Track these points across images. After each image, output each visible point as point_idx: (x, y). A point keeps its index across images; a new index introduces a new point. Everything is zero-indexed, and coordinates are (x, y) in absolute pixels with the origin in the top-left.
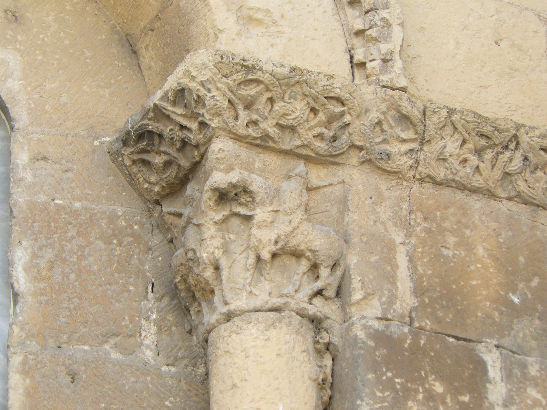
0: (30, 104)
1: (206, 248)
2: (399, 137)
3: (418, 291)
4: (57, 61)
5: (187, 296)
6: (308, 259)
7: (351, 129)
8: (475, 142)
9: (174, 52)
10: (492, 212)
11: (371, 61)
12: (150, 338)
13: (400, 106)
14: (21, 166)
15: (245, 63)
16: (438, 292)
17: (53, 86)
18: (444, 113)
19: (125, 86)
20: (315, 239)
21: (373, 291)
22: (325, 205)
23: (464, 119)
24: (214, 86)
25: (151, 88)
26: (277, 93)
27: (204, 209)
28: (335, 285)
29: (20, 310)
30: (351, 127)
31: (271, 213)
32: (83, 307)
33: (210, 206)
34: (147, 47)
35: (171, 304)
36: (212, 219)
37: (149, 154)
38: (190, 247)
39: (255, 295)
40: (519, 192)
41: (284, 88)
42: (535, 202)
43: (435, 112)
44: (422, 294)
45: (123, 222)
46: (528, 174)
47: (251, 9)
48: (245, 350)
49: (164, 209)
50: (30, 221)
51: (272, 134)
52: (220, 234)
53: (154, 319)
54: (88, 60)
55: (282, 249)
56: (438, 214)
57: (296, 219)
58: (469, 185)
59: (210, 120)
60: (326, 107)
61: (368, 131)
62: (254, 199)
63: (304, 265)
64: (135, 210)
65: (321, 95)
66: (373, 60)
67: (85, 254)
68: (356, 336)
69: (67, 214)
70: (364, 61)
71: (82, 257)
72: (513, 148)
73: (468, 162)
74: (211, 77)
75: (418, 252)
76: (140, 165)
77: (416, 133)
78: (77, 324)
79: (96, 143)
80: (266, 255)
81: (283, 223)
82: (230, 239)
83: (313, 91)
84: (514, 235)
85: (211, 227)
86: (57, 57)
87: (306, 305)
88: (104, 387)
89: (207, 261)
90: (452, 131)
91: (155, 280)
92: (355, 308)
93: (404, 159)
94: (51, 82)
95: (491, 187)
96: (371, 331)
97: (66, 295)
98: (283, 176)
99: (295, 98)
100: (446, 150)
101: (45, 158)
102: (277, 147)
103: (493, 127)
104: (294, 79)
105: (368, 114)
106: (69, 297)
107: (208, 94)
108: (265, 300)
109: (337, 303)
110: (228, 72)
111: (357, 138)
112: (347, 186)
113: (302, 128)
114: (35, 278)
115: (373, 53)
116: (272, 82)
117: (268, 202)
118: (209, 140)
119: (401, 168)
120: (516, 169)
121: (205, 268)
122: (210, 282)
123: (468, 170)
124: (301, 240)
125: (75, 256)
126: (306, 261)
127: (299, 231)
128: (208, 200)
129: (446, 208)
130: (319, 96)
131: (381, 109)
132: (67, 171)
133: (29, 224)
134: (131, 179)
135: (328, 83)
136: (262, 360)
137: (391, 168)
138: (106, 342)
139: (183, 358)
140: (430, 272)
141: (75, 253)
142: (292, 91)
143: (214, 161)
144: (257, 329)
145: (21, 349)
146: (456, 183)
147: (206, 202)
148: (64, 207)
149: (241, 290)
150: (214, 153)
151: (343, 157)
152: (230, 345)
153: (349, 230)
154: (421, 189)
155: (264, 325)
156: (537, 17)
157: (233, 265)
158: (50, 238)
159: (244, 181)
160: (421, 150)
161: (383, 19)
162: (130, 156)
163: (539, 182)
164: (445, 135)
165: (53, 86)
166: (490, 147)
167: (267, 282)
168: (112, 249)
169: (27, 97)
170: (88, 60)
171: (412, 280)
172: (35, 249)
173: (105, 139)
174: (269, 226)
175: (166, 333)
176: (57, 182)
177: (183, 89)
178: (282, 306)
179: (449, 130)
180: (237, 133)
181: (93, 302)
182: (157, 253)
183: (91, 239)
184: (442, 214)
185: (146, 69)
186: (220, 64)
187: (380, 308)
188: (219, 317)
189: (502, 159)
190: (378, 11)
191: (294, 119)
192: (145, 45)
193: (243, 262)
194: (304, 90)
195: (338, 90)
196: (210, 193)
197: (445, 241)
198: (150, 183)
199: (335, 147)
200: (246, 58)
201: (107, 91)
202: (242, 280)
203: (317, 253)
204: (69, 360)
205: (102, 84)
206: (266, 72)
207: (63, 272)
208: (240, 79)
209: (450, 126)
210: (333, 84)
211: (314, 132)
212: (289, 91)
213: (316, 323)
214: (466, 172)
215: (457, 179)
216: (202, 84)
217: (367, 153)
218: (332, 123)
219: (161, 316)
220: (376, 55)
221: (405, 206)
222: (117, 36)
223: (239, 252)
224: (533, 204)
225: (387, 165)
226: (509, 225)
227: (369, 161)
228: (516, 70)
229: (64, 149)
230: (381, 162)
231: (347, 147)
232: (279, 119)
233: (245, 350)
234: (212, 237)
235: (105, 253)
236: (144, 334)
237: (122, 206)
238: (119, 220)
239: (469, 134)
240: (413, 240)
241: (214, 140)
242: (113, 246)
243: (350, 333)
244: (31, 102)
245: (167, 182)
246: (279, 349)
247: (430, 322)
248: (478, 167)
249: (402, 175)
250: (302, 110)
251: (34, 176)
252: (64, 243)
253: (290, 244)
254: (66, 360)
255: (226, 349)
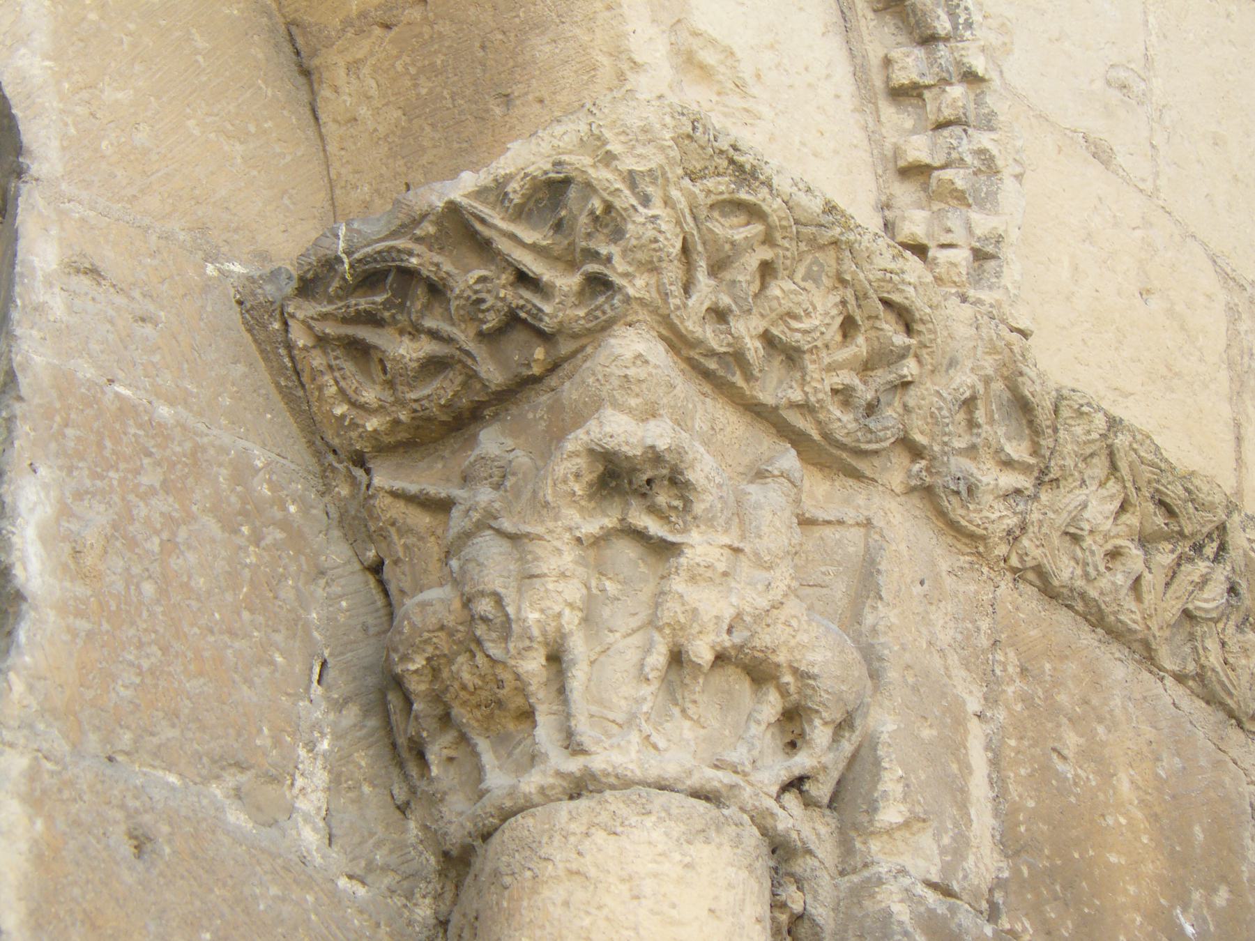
0: (66, 124)
1: (541, 599)
2: (1002, 450)
3: (1010, 844)
4: (130, 38)
5: (432, 712)
6: (784, 692)
7: (912, 397)
8: (1147, 515)
9: (453, 97)
10: (1145, 698)
11: (943, 246)
12: (313, 797)
13: (1021, 374)
14: (40, 273)
15: (738, 158)
16: (1048, 857)
17: (120, 95)
18: (1100, 422)
19: (278, 150)
20: (811, 645)
21: (925, 812)
22: (823, 569)
23: (1135, 451)
24: (660, 193)
25: (343, 171)
26: (788, 254)
27: (550, 498)
28: (836, 775)
29: (28, 637)
30: (912, 391)
31: (727, 552)
32: (169, 673)
33: (574, 494)
34: (353, 67)
35: (364, 726)
36: (570, 529)
37: (379, 331)
38: (490, 587)
39: (655, 747)
40: (1202, 667)
41: (803, 247)
42: (1229, 701)
43: (1081, 414)
44: (1017, 853)
45: (265, 486)
46: (1231, 629)
47: (696, 34)
48: (631, 878)
49: (377, 481)
50: (58, 418)
51: (751, 356)
52: (581, 570)
53: (325, 751)
54: (200, 58)
55: (740, 648)
56: (1048, 666)
57: (778, 583)
58: (1112, 618)
59: (626, 275)
60: (878, 324)
61: (945, 412)
62: (687, 503)
63: (771, 706)
64: (293, 466)
65: (876, 291)
66: (950, 246)
67: (179, 540)
68: (888, 915)
69: (140, 426)
70: (925, 241)
71: (170, 547)
72: (1212, 557)
73: (1122, 559)
74: (662, 167)
75: (1009, 746)
76: (338, 353)
77: (1035, 453)
78: (156, 713)
79: (210, 270)
80: (702, 652)
81: (752, 584)
82: (603, 590)
83: (861, 276)
84: (1184, 768)
85: (565, 548)
86: (132, 27)
87: (771, 804)
88: (211, 890)
89: (536, 632)
90: (1106, 471)
91: (331, 655)
92: (878, 844)
93: (1000, 509)
94: (115, 84)
95: (1154, 636)
96: (922, 909)
97: (132, 632)
98: (741, 469)
99: (816, 281)
100: (1086, 515)
101: (94, 272)
102: (748, 393)
103: (1186, 489)
104: (830, 233)
105: (951, 372)
106: (140, 639)
107: (641, 209)
108: (688, 765)
109: (828, 819)
110: (699, 167)
111: (920, 423)
112: (877, 537)
113: (815, 362)
114: (65, 567)
115: (953, 228)
116: (784, 223)
117: (722, 521)
118: (602, 328)
119: (990, 527)
120: (1213, 609)
121: (529, 648)
122: (533, 688)
123: (1120, 579)
124: (783, 639)
125: (156, 540)
126: (777, 695)
127: (783, 614)
128: (571, 478)
129: (1064, 658)
130: (871, 292)
131: (983, 368)
132: (143, 320)
133: (55, 426)
134: (295, 387)
135: (892, 266)
136: (674, 913)
137: (970, 522)
138: (218, 777)
139: (385, 869)
140: (1031, 804)
141: (157, 533)
142: (816, 261)
143: (616, 382)
144: (666, 834)
145: (27, 738)
146: (1086, 605)
147: (565, 481)
148: (134, 407)
149: (620, 726)
150: (619, 363)
151: (876, 462)
152: (588, 857)
153: (878, 647)
154: (1016, 595)
155: (683, 828)
156: (1210, 263)
157: (603, 658)
158: (102, 478)
159: (680, 452)
160: (1035, 498)
161: (981, 152)
162: (313, 323)
163: (1248, 657)
164: (1089, 477)
165: (120, 95)
166: (1168, 538)
167: (687, 723)
168: (240, 548)
169: (61, 106)
170: (200, 58)
171: (997, 813)
172: (68, 494)
173: (232, 267)
174: (718, 581)
175: (350, 795)
176: (122, 341)
177: (567, 182)
178: (724, 791)
179: (1099, 467)
180: (681, 327)
181: (192, 667)
182: (336, 589)
183: (194, 508)
184: (1055, 669)
185: (335, 121)
186: (686, 142)
187: (937, 860)
188: (551, 780)
189: (1189, 574)
190: (970, 131)
191: (806, 332)
192: (350, 58)
193: (633, 656)
194: (845, 267)
195: (911, 289)
196: (582, 462)
197: (1060, 739)
198: (354, 404)
199: (871, 432)
200: (740, 145)
201: (238, 147)
202: (623, 703)
203: (811, 682)
204: (136, 798)
205: (230, 127)
206: (778, 195)
207: (128, 570)
208: (722, 193)
209: (1103, 458)
210: (903, 272)
211: (836, 380)
212: (808, 259)
213: (781, 853)
214: (1113, 583)
215: (1093, 594)
216: (631, 179)
217: (928, 469)
218: (873, 370)
219: (341, 749)
220: (959, 236)
221: (985, 624)
222: (265, 20)
223: (623, 630)
224: (1222, 705)
225: (963, 512)
226: (1176, 742)
227: (928, 491)
228: (1176, 374)
229: (140, 262)
230: (953, 499)
231: (892, 440)
232: (773, 323)
233: (631, 878)
234: (563, 575)
235: (223, 553)
236: (300, 782)
237: (264, 446)
238: (256, 480)
239: (1138, 489)
240: (1001, 715)
241: (619, 329)
242: (241, 541)
243: (866, 903)
244: (70, 121)
245: (415, 411)
246: (716, 898)
247: (1031, 925)
248: (1138, 580)
249: (986, 547)
250: (827, 314)
251: (71, 310)
252: (131, 497)
253: (757, 643)
254: (129, 795)
255: (574, 867)
